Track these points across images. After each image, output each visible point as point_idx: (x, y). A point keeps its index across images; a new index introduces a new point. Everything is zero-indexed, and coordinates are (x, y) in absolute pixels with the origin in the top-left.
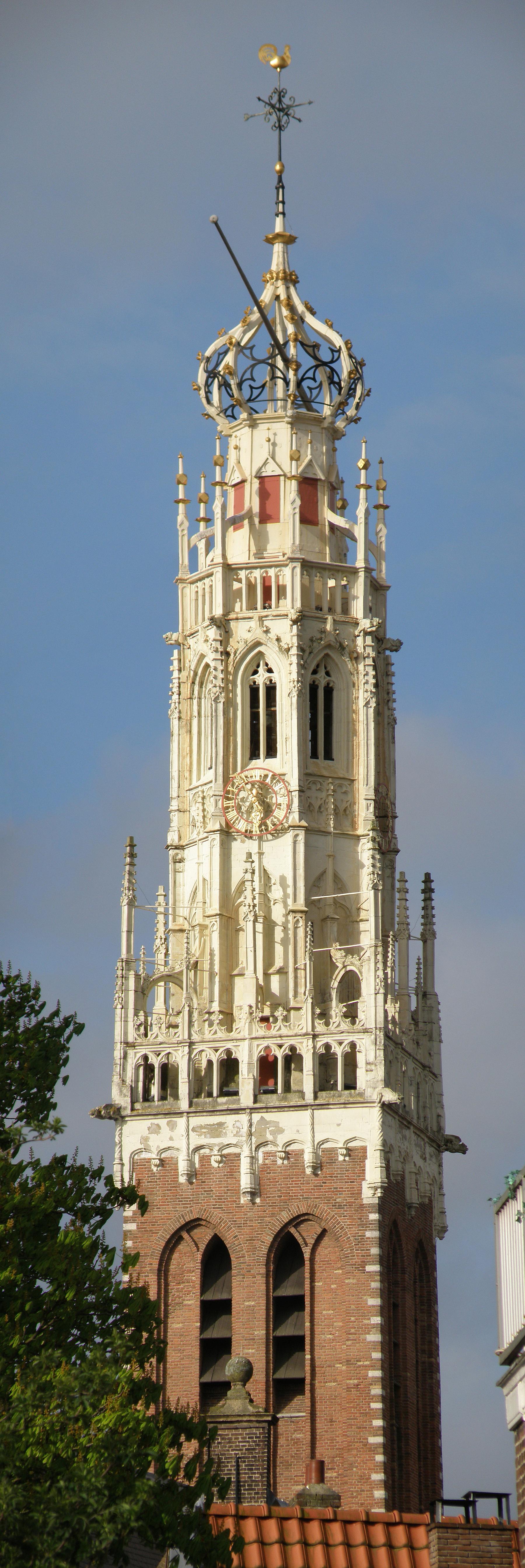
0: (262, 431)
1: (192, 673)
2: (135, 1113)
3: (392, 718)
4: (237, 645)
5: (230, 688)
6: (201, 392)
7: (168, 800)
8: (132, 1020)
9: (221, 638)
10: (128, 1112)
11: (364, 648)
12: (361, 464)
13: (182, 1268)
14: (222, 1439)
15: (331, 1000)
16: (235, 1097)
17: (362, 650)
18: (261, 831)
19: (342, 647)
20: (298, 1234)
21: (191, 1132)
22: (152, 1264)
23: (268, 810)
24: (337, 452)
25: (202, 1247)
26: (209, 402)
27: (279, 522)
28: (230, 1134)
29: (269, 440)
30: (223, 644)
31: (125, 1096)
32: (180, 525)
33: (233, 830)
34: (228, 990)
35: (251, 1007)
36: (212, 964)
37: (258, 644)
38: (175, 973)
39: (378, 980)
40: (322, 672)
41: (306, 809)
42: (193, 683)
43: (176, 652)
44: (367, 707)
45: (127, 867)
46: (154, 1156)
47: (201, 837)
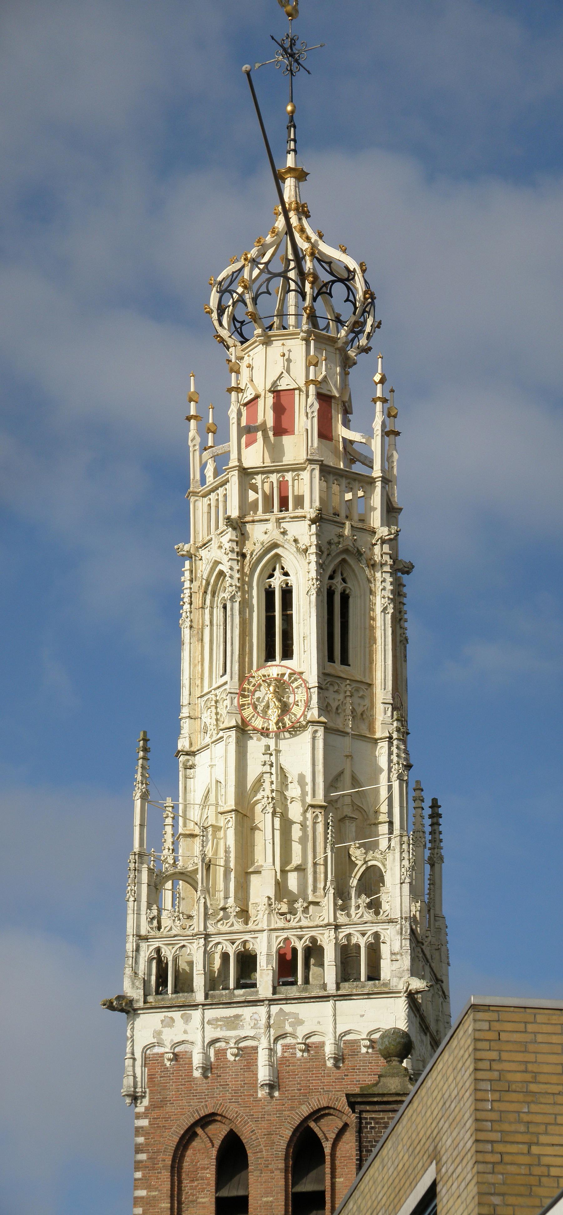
0: (277, 347)
1: (204, 582)
2: (148, 1005)
3: (404, 636)
4: (252, 547)
5: (246, 589)
6: (213, 315)
7: (178, 708)
8: (145, 913)
9: (237, 539)
10: (141, 1004)
11: (382, 556)
12: (377, 378)
13: (196, 1165)
14: (377, 1123)
15: (351, 899)
16: (252, 989)
17: (380, 558)
18: (279, 728)
19: (360, 554)
20: (318, 1128)
21: (206, 1025)
22: (165, 1161)
23: (285, 708)
24: (350, 376)
25: (218, 1143)
26: (221, 324)
27: (294, 434)
28: (247, 1027)
29: (284, 355)
30: (239, 544)
31: (137, 988)
32: (192, 441)
33: (250, 728)
34: (243, 889)
35: (269, 898)
36: (227, 861)
37: (275, 545)
38: (188, 871)
39: (403, 870)
40: (338, 579)
41: (324, 708)
42: (205, 592)
43: (187, 563)
44: (385, 613)
45: (140, 761)
46: (167, 1050)
47: (214, 739)
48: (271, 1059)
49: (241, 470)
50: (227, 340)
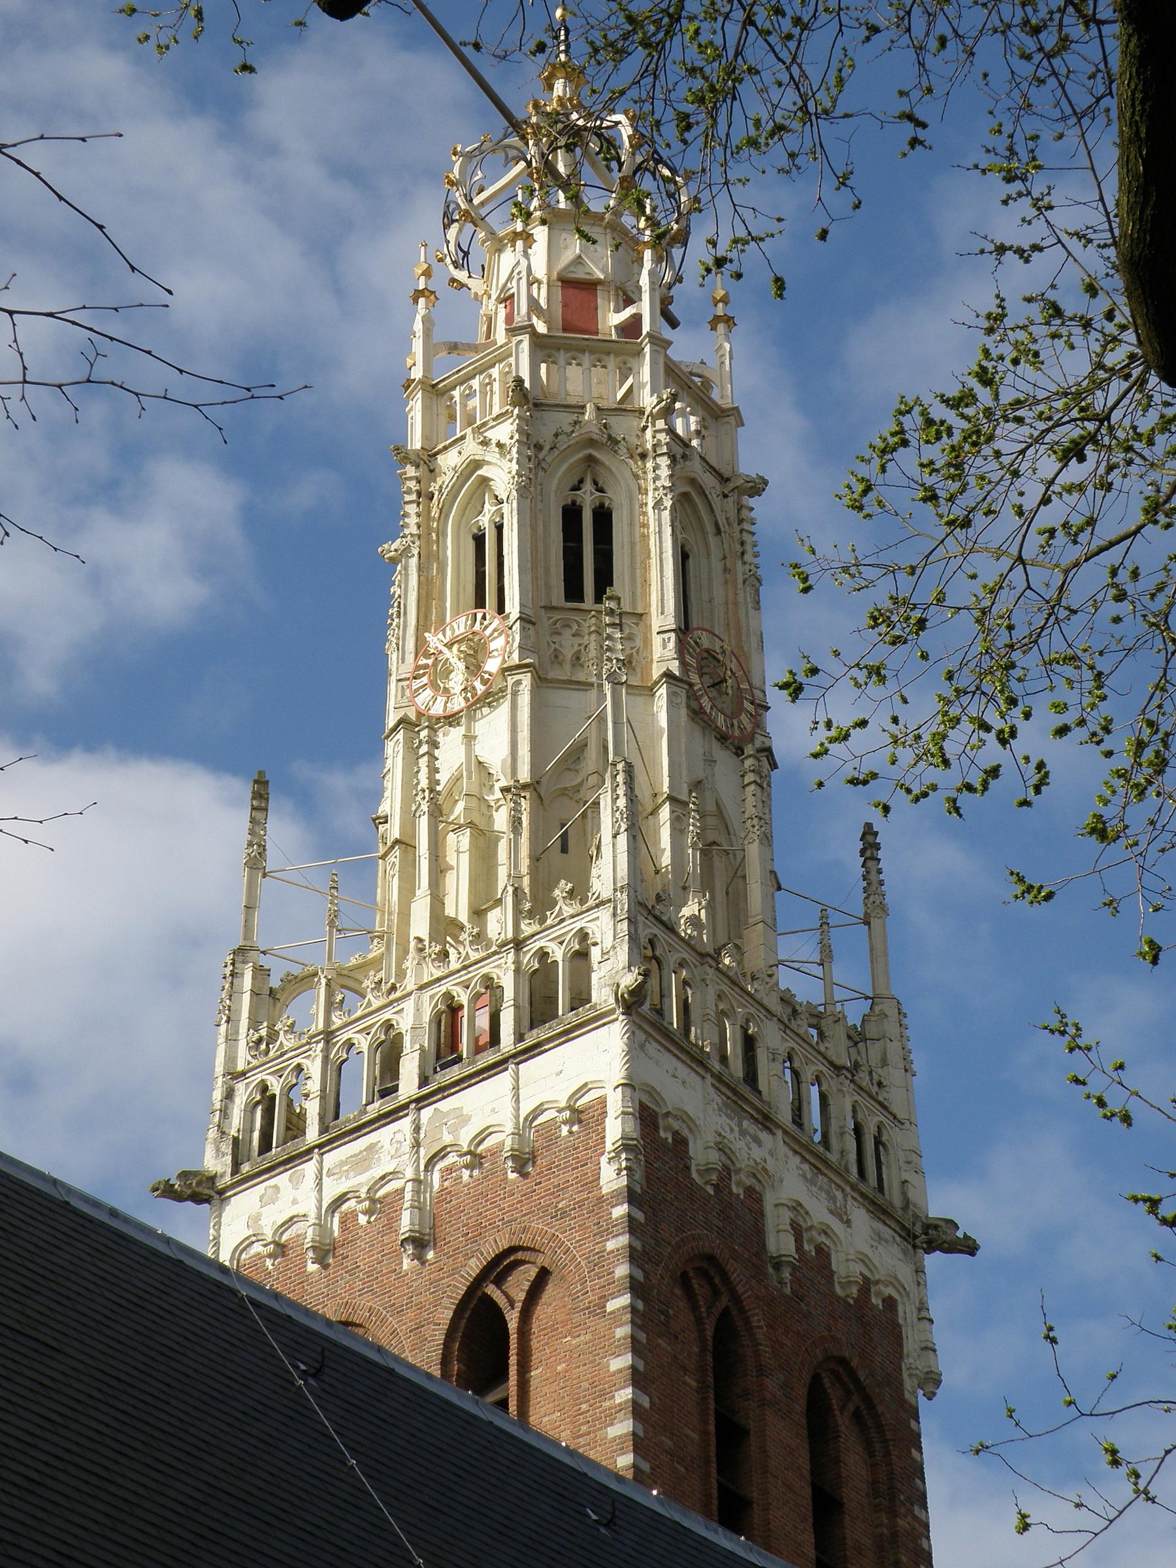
40: (588, 486)
48: (419, 1197)
49: (429, 389)
50: (467, 282)
